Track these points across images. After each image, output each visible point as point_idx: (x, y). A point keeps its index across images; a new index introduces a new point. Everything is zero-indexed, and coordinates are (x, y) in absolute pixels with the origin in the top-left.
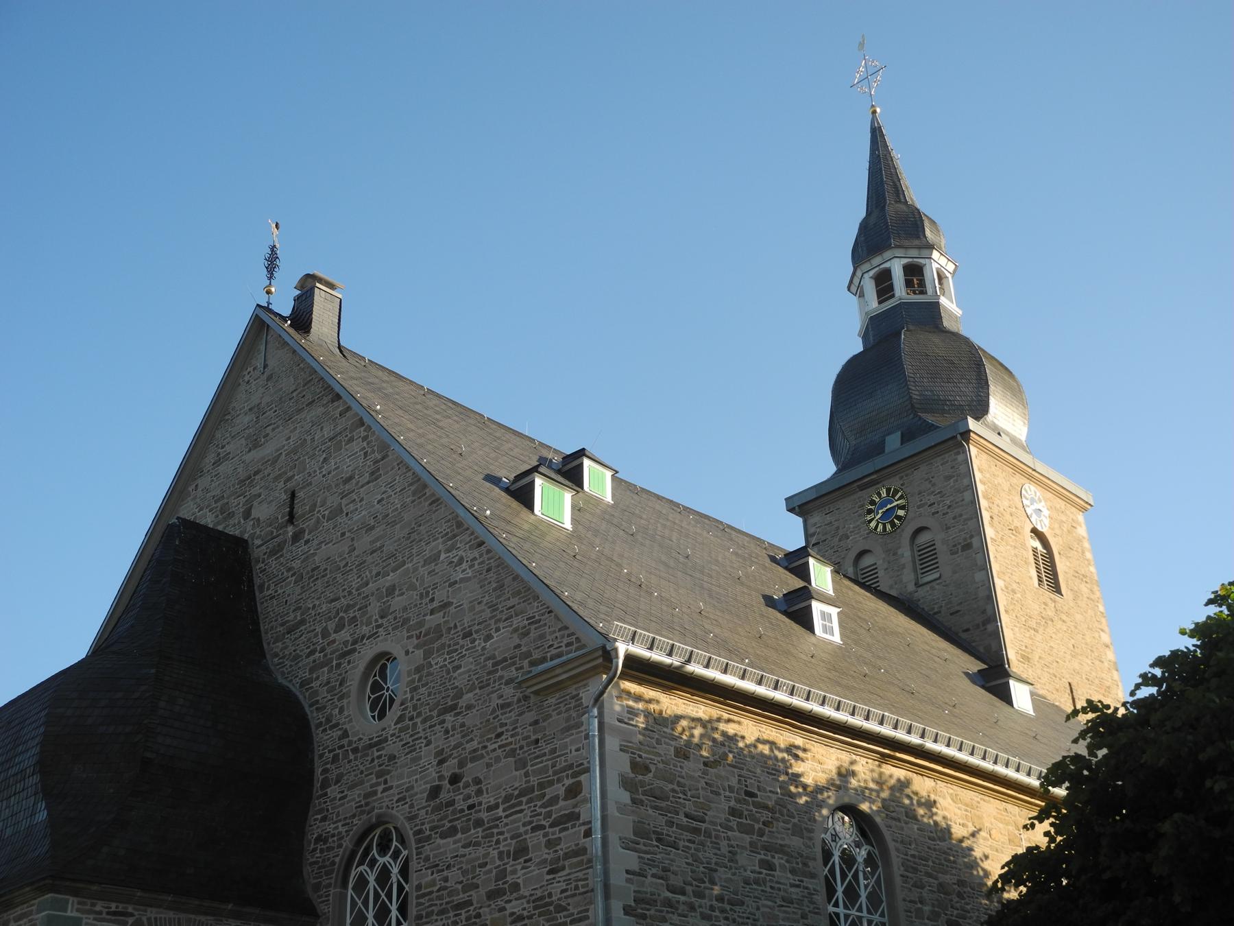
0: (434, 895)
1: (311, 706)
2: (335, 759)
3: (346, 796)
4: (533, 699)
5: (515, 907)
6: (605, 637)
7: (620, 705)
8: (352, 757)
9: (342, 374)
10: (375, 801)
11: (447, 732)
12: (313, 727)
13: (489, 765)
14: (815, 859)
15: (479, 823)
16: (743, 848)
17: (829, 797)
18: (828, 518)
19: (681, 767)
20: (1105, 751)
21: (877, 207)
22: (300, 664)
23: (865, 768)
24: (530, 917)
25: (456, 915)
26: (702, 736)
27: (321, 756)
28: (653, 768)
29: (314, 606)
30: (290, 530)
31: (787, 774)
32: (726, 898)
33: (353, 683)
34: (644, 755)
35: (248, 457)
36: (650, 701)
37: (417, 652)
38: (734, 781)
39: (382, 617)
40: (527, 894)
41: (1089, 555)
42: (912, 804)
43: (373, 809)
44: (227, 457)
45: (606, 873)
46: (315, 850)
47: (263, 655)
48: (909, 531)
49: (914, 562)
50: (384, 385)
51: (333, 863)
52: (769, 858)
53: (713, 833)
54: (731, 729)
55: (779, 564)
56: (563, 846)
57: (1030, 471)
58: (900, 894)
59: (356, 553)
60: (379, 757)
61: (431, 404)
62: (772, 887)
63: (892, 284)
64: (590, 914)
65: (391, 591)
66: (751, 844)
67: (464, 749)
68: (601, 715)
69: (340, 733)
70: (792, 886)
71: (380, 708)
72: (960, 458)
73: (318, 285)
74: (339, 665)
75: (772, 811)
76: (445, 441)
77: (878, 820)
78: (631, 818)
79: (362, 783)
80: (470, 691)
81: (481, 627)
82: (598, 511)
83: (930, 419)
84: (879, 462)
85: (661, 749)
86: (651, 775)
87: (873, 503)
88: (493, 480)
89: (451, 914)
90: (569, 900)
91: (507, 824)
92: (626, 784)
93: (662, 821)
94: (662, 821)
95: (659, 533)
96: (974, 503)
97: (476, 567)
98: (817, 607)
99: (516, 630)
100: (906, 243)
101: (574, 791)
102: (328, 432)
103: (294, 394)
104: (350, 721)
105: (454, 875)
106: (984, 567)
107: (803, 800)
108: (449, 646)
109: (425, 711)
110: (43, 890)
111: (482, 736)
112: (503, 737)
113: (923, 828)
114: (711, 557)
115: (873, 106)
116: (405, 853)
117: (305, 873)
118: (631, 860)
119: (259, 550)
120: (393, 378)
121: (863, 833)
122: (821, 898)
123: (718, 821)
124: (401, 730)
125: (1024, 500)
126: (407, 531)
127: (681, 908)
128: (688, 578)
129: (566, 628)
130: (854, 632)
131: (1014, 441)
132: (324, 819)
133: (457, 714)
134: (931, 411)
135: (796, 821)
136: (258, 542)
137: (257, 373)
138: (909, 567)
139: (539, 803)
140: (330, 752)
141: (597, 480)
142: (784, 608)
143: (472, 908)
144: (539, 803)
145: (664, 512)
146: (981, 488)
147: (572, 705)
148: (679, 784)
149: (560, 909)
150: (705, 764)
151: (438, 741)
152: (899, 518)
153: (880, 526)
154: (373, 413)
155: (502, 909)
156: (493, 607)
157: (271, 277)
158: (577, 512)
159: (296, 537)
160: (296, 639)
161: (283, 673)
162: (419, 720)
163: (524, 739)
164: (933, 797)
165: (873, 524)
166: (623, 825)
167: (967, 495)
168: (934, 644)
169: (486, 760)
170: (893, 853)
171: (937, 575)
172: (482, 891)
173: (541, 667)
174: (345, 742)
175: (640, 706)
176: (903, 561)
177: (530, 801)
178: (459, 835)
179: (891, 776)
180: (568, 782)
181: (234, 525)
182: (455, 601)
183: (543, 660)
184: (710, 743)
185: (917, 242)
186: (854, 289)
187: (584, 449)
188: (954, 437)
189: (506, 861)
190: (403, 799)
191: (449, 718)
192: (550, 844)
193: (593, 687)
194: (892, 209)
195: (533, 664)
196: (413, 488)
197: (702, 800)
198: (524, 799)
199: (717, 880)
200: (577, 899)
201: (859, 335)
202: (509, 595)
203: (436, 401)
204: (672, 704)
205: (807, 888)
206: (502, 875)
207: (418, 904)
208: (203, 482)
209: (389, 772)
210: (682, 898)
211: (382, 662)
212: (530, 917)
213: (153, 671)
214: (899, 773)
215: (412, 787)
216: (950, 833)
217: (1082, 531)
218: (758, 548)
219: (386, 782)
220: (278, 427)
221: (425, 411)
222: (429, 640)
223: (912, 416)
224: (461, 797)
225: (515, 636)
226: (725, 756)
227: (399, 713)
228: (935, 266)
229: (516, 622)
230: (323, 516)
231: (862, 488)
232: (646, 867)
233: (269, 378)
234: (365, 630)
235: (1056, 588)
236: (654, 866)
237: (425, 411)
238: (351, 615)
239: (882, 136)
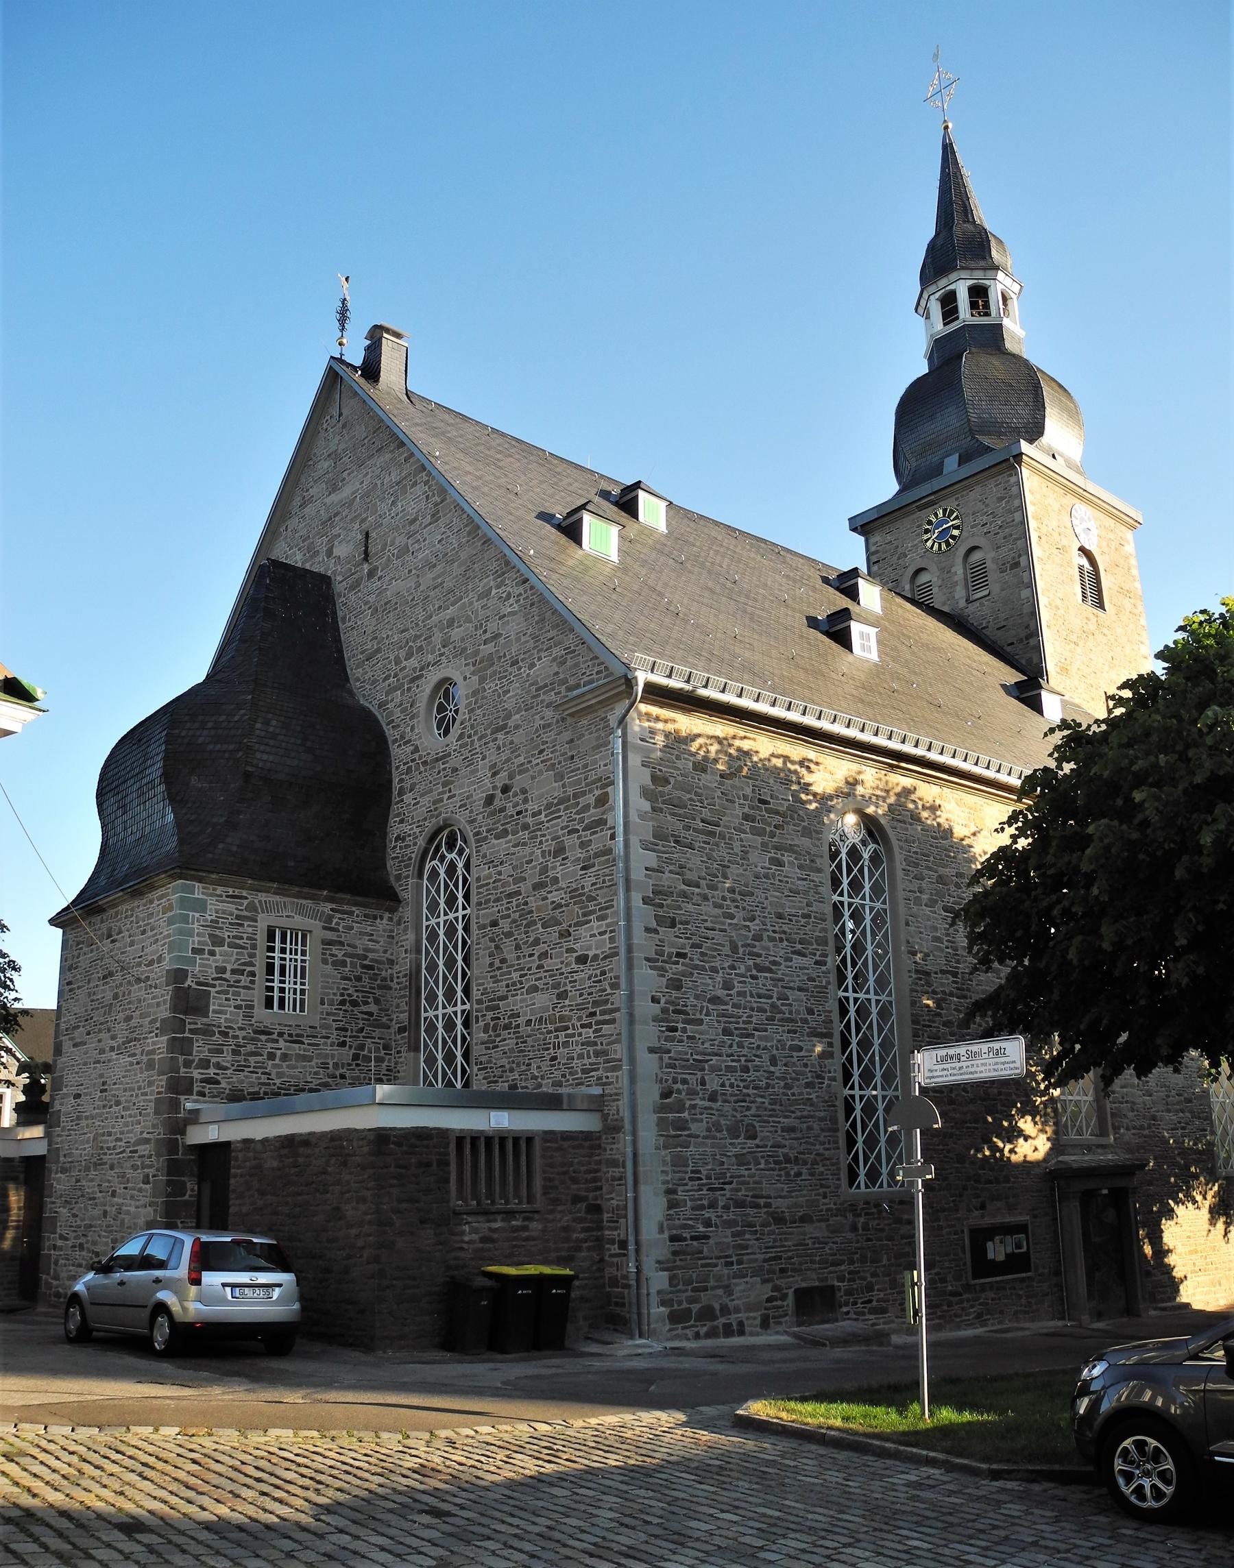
0: (491, 886)
1: (388, 724)
2: (409, 770)
3: (418, 803)
4: (569, 720)
5: (555, 897)
6: (627, 666)
7: (640, 726)
8: (422, 769)
9: (407, 424)
10: (442, 807)
11: (499, 748)
12: (390, 743)
13: (533, 778)
14: (822, 857)
15: (525, 827)
16: (756, 848)
17: (838, 803)
18: (889, 538)
19: (699, 779)
20: (1072, 765)
21: (945, 227)
22: (378, 688)
23: (871, 776)
24: (567, 905)
25: (508, 903)
26: (717, 752)
27: (397, 768)
28: (672, 781)
29: (388, 636)
30: (366, 567)
31: (799, 783)
32: (737, 890)
33: (422, 704)
34: (664, 769)
35: (328, 501)
36: (666, 721)
37: (473, 678)
38: (748, 791)
39: (444, 647)
40: (564, 886)
41: (1135, 572)
42: (917, 808)
43: (440, 814)
44: (310, 500)
45: (627, 869)
46: (395, 847)
47: (347, 680)
48: (962, 551)
49: (966, 580)
50: (449, 428)
51: (410, 858)
52: (779, 856)
53: (727, 836)
54: (746, 745)
55: (830, 585)
56: (593, 846)
57: (1081, 491)
58: (900, 886)
59: (421, 588)
60: (444, 769)
61: (494, 444)
62: (780, 880)
63: (957, 306)
64: (614, 903)
65: (451, 623)
66: (763, 844)
67: (513, 763)
68: (624, 735)
69: (412, 748)
70: (799, 879)
71: (445, 727)
72: (1013, 479)
73: (385, 335)
74: (409, 689)
75: (783, 815)
76: (502, 481)
77: (883, 821)
78: (651, 823)
79: (431, 791)
80: (518, 712)
81: (526, 656)
82: (650, 541)
83: (986, 441)
84: (937, 483)
85: (679, 764)
86: (670, 786)
87: (930, 523)
88: (545, 517)
89: (505, 902)
90: (598, 892)
91: (548, 828)
92: (646, 794)
93: (680, 825)
94: (680, 825)
95: (709, 559)
96: (1023, 524)
97: (522, 602)
98: (856, 628)
99: (554, 659)
100: (973, 264)
101: (603, 801)
102: (394, 477)
103: (366, 441)
104: (420, 738)
105: (506, 869)
106: (1031, 585)
107: (813, 806)
108: (500, 672)
109: (481, 729)
110: (174, 877)
111: (527, 752)
112: (545, 753)
113: (926, 829)
114: (760, 581)
115: (945, 121)
116: (467, 850)
117: (388, 866)
118: (651, 859)
119: (339, 587)
120: (458, 420)
121: (870, 833)
122: (826, 888)
123: (732, 825)
124: (461, 747)
125: (1073, 519)
126: (463, 568)
127: (695, 898)
128: (732, 603)
129: (597, 658)
130: (894, 649)
131: (1069, 464)
132: (402, 821)
133: (507, 733)
134: (989, 433)
135: (806, 824)
136: (339, 578)
137: (334, 421)
138: (962, 583)
139: (574, 811)
140: (404, 764)
141: (651, 511)
142: (826, 628)
143: (521, 897)
144: (574, 811)
145: (720, 538)
146: (1031, 510)
147: (601, 726)
148: (696, 794)
149: (591, 899)
150: (722, 776)
151: (492, 756)
152: (953, 537)
153: (936, 545)
154: (432, 460)
155: (545, 898)
156: (535, 638)
157: (343, 329)
158: (627, 544)
159: (371, 574)
160: (374, 665)
161: (364, 696)
162: (476, 738)
163: (562, 755)
164: (938, 802)
165: (929, 544)
166: (644, 830)
167: (1017, 516)
168: (976, 658)
169: (531, 773)
170: (896, 850)
171: (986, 592)
172: (529, 883)
173: (575, 693)
174: (416, 756)
175: (660, 726)
176: (956, 578)
177: (566, 808)
178: (510, 837)
179: (897, 784)
180: (597, 793)
181: (319, 563)
182: (504, 633)
183: (577, 686)
184: (727, 758)
185: (982, 263)
186: (921, 310)
187: (640, 482)
188: (1008, 460)
189: (548, 858)
190: (465, 805)
191: (500, 736)
192: (583, 845)
193: (619, 709)
194: (959, 228)
195: (569, 689)
196: (468, 529)
197: (717, 807)
198: (562, 807)
199: (729, 875)
200: (605, 890)
201: (925, 357)
202: (548, 628)
203: (500, 440)
204: (686, 723)
205: (813, 881)
206: (544, 870)
207: (479, 893)
208: (293, 523)
209: (453, 782)
210: (697, 890)
211: (444, 688)
212: (567, 905)
213: (250, 697)
214: (907, 782)
215: (471, 795)
216: (952, 833)
217: (1130, 548)
218: (812, 570)
219: (450, 791)
220: (353, 472)
221: (487, 452)
222: (483, 666)
223: (969, 439)
224: (511, 804)
225: (554, 664)
226: (740, 769)
227: (460, 732)
228: (1000, 287)
229: (557, 652)
230: (393, 555)
231: (921, 508)
232: (664, 865)
233: (344, 426)
234: (430, 658)
235: (1101, 605)
236: (671, 864)
237: (487, 452)
238: (419, 645)
239: (953, 153)
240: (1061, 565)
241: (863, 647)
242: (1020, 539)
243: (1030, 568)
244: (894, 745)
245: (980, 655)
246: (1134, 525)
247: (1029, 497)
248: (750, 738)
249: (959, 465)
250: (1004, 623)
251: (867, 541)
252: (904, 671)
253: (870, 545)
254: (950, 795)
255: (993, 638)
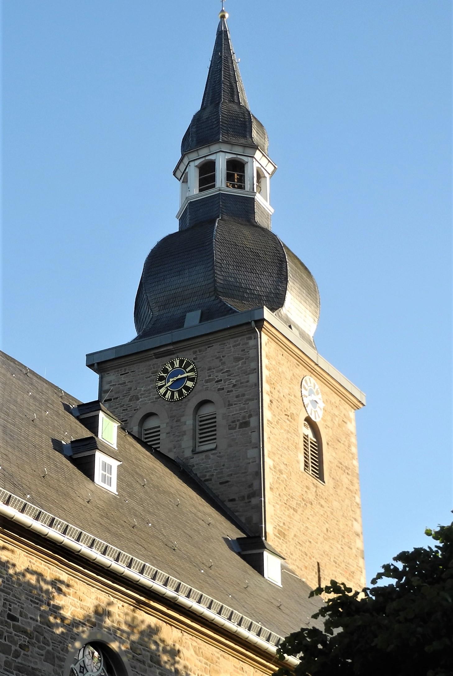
17: (83, 632)
18: (123, 379)
20: (340, 630)
21: (211, 103)
31: (49, 604)
41: (354, 450)
42: (158, 650)
49: (194, 430)
57: (313, 364)
72: (252, 343)
75: (30, 636)
77: (124, 659)
83: (230, 303)
84: (177, 335)
87: (165, 371)
98: (100, 458)
100: (233, 140)
107: (59, 631)
114: (11, 397)
115: (222, 11)
125: (303, 390)
130: (130, 485)
131: (303, 335)
134: (232, 296)
135: (50, 648)
138: (190, 434)
142: (70, 453)
152: (187, 388)
164: (178, 647)
165: (162, 391)
167: (252, 377)
168: (201, 508)
171: (213, 446)
176: (185, 428)
179: (143, 622)
185: (242, 141)
186: (179, 174)
188: (249, 323)
194: (225, 107)
201: (177, 217)
214: (151, 620)
217: (351, 427)
218: (55, 396)
228: (256, 165)
231: (158, 356)
235: (320, 476)
239: (227, 39)
240: (288, 432)
241: (104, 479)
242: (253, 400)
243: (259, 429)
244: (145, 580)
245: (203, 506)
246: (357, 405)
247: (265, 362)
248: (7, 549)
249: (200, 322)
250: (227, 479)
251: (101, 379)
252: (139, 509)
253: (104, 383)
254: (189, 642)
255: (215, 492)
